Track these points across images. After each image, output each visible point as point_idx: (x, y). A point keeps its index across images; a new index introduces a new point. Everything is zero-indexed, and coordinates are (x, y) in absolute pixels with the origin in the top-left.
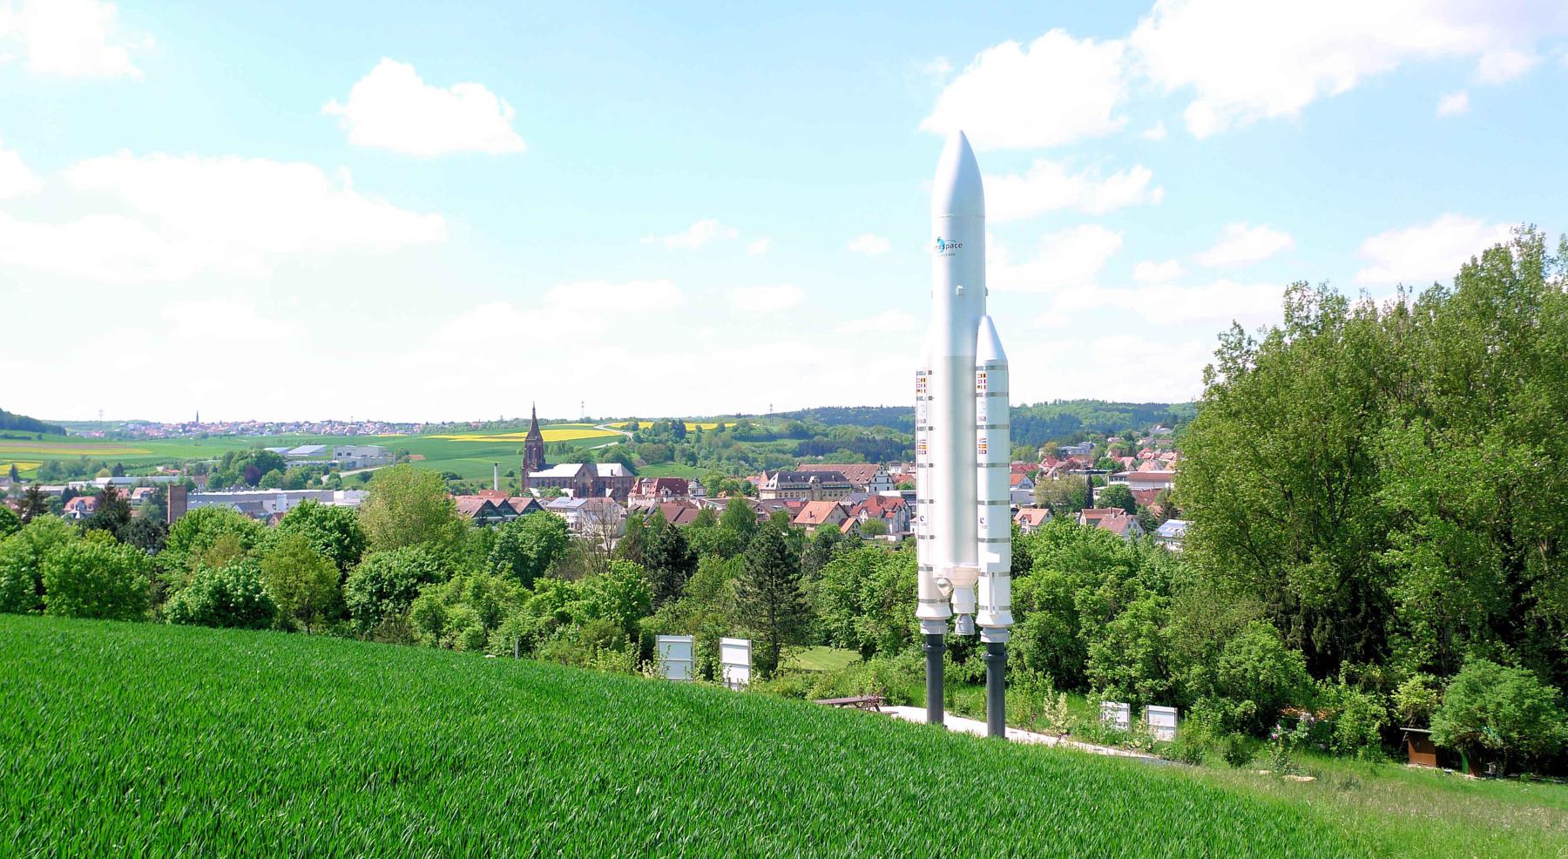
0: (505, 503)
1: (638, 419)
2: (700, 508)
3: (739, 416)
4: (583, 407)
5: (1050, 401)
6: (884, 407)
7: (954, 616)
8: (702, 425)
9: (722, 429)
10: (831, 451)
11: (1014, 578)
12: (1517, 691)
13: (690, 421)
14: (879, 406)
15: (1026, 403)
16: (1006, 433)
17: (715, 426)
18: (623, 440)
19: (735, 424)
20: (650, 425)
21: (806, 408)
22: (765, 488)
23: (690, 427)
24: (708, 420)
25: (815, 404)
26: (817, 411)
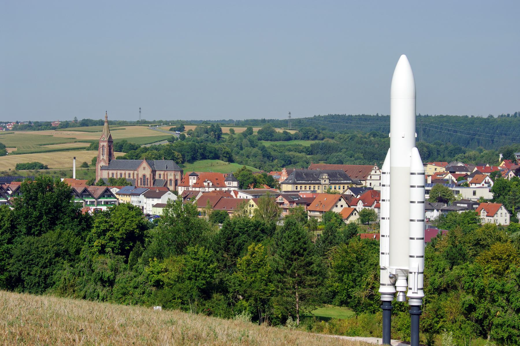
0: (85, 190)
1: (183, 122)
2: (235, 197)
3: (264, 121)
4: (140, 112)
5: (512, 113)
6: (380, 115)
7: (397, 292)
8: (235, 129)
9: (250, 132)
10: (336, 151)
11: (148, 228)
12: (46, 290)
13: (225, 123)
14: (375, 115)
15: (492, 114)
16: (288, 118)
17: (245, 129)
18: (172, 140)
19: (261, 128)
20: (193, 128)
21: (317, 115)
22: (327, 185)
23: (225, 130)
24: (239, 124)
25: (324, 112)
26: (325, 117)
